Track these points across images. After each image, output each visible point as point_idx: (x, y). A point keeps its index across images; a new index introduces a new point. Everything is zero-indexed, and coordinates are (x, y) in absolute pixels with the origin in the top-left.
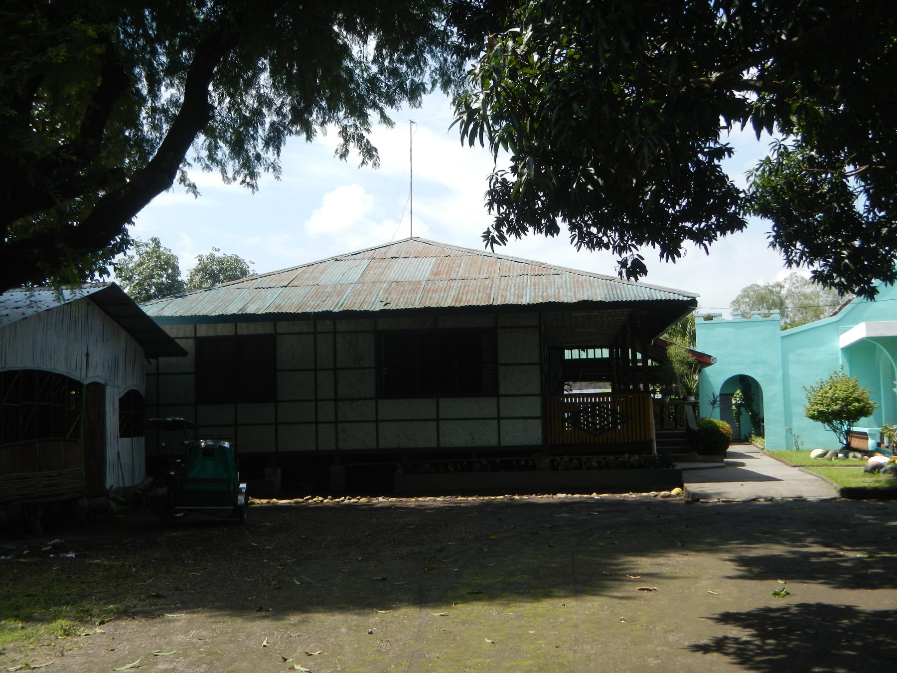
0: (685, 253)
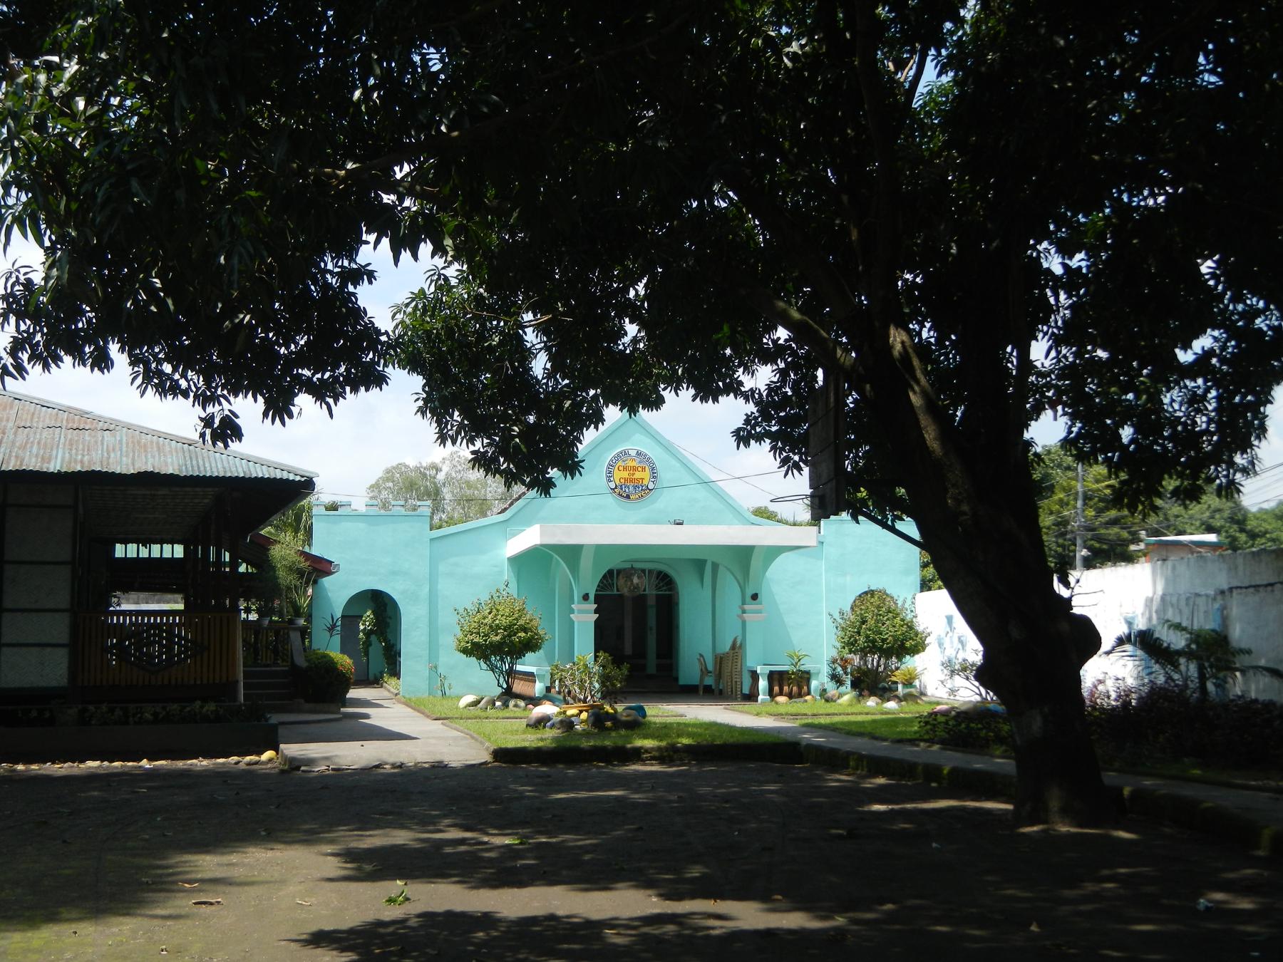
0: (300, 413)
